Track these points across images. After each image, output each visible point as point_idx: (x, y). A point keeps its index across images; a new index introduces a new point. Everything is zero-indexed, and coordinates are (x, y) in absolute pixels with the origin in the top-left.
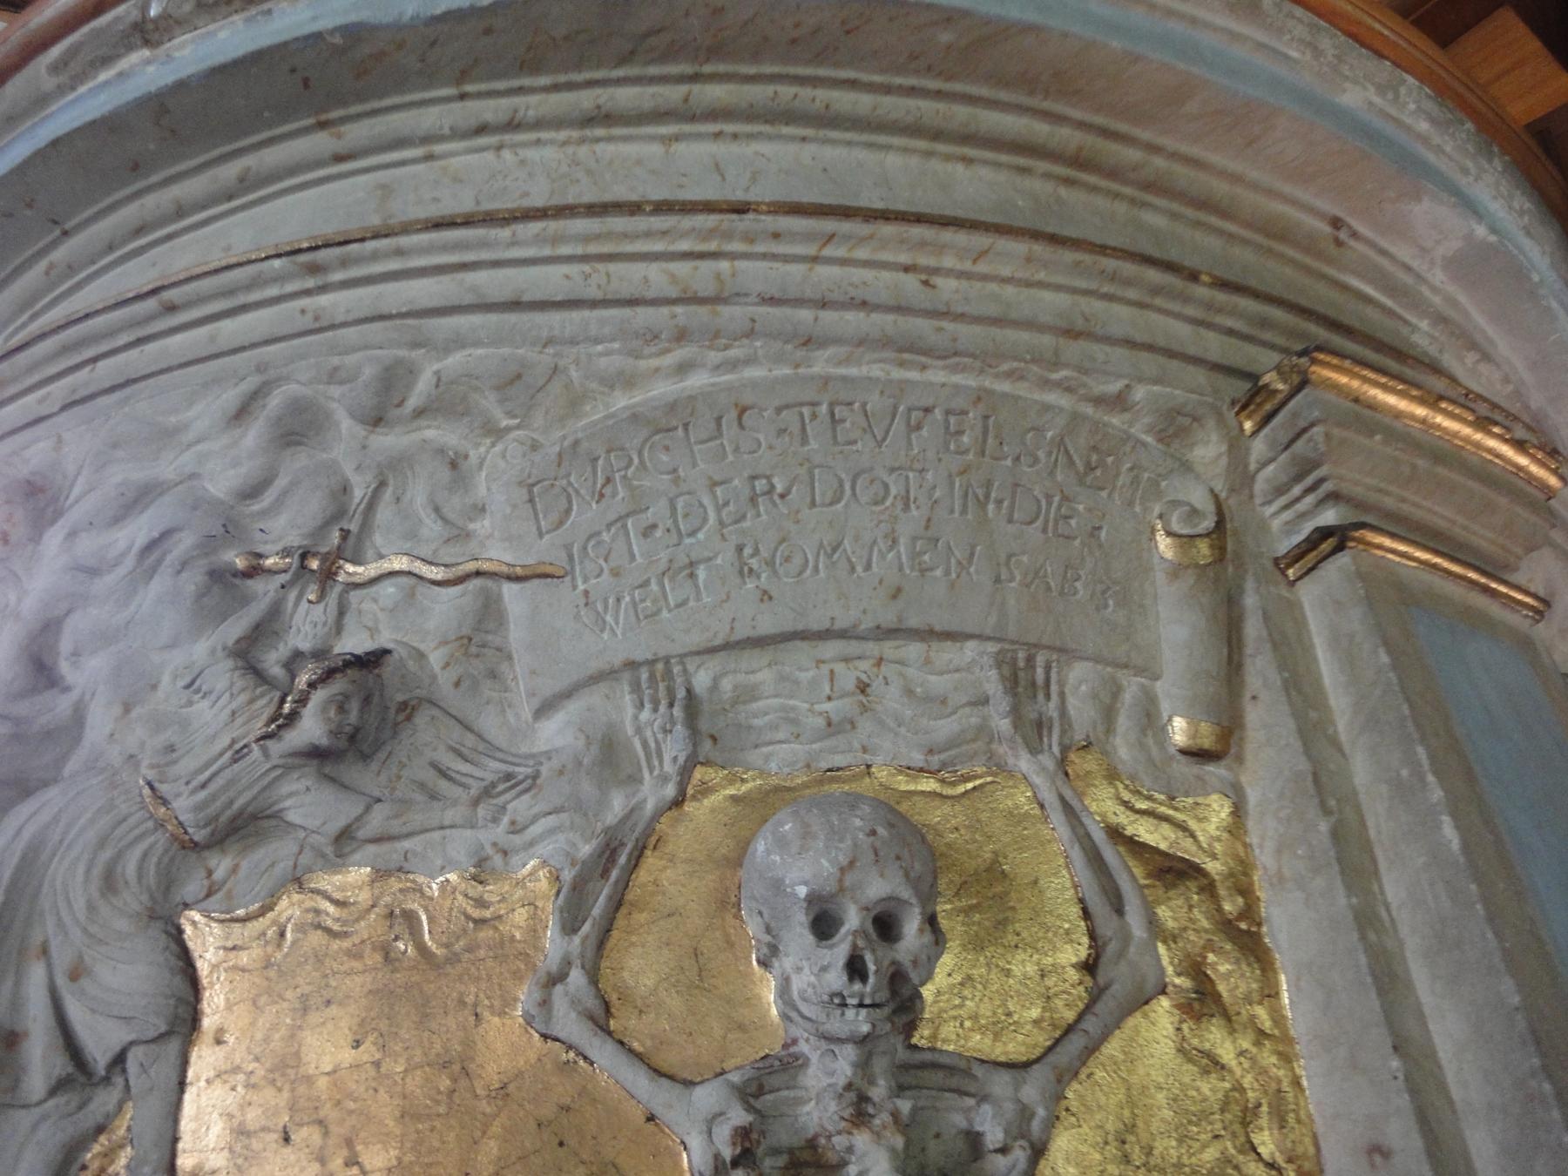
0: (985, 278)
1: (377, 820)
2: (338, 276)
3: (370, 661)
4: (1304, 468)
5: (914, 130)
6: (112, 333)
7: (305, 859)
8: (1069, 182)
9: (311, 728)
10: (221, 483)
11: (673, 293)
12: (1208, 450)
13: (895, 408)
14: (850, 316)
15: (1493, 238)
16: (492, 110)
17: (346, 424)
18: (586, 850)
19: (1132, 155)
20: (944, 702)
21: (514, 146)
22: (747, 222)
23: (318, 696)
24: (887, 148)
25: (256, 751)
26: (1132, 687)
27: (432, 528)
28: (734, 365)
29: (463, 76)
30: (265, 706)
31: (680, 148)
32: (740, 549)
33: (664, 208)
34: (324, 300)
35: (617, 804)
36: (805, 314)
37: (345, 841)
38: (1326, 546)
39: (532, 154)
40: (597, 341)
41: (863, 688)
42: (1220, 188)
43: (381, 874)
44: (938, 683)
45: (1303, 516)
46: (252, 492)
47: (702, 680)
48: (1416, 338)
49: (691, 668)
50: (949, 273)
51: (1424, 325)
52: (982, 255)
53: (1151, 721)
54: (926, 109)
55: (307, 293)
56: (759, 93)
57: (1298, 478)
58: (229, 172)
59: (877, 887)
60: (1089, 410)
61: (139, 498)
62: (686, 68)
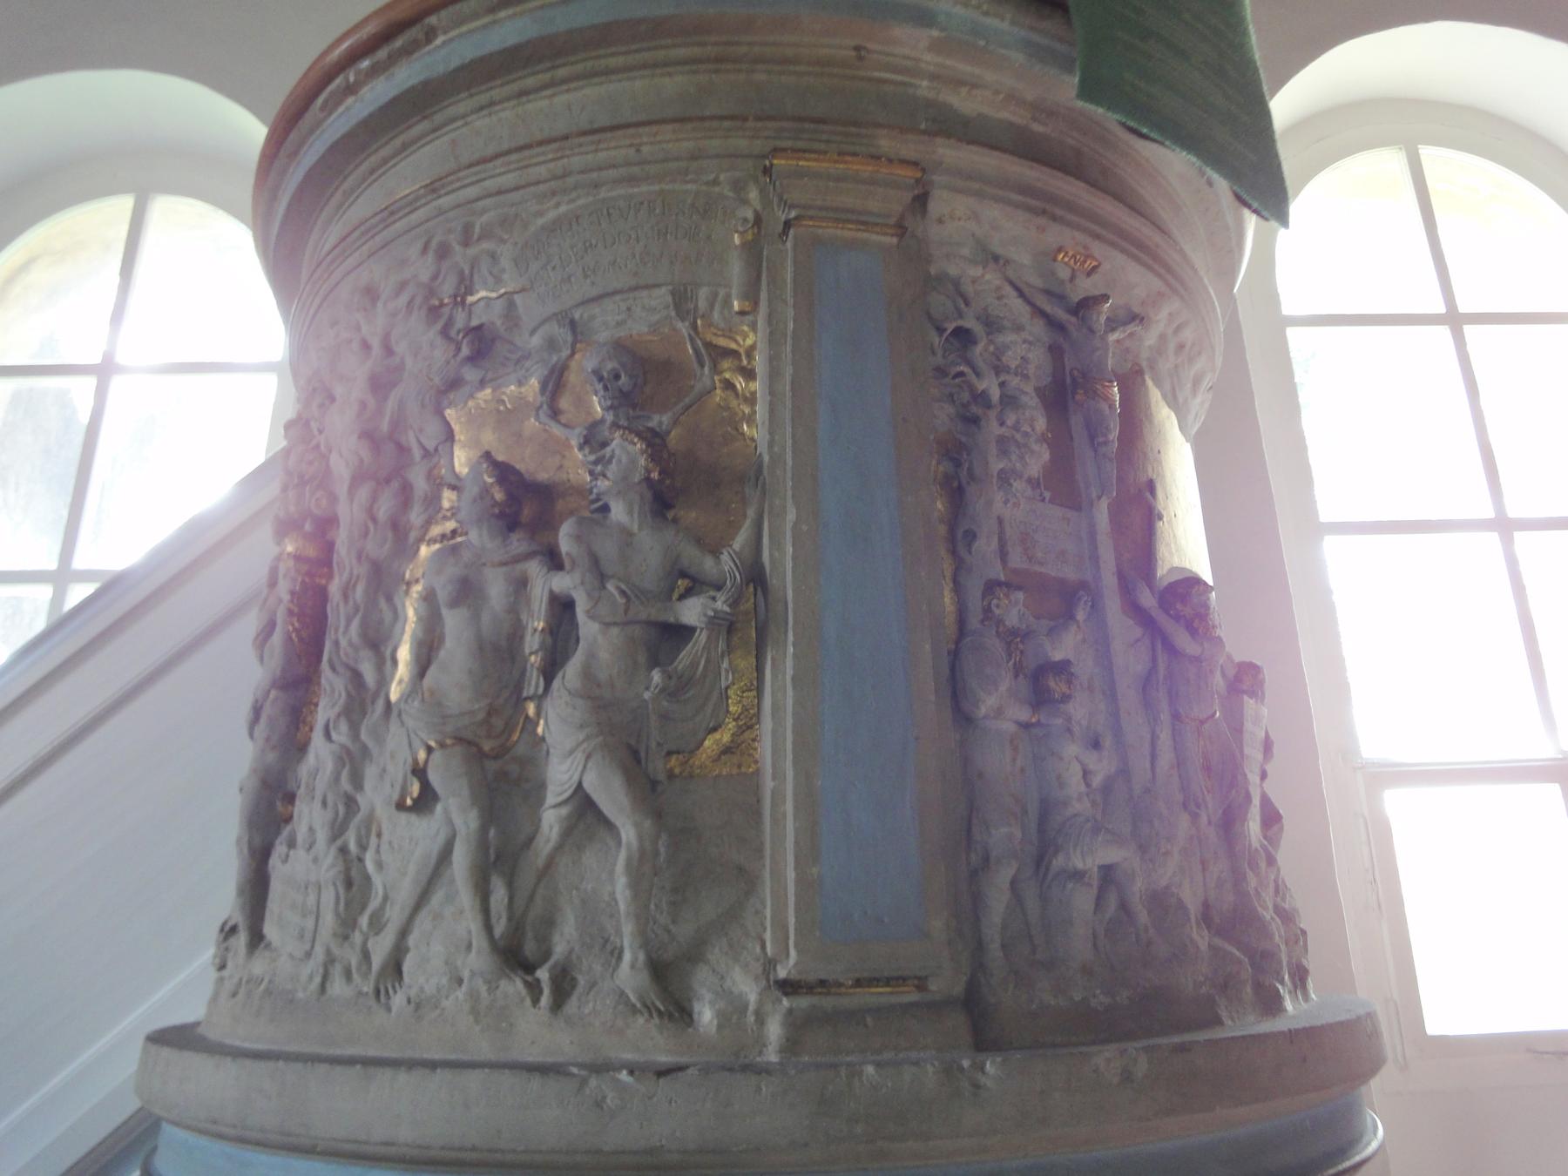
0: (660, 142)
2: (443, 192)
3: (479, 328)
5: (644, 66)
6: (377, 225)
8: (717, 71)
9: (465, 351)
10: (425, 277)
12: (753, 194)
13: (630, 205)
14: (610, 172)
15: (943, 34)
16: (483, 99)
17: (458, 248)
18: (546, 373)
19: (743, 49)
20: (655, 309)
23: (465, 341)
25: (452, 361)
26: (722, 292)
27: (491, 280)
28: (573, 201)
30: (453, 347)
31: (556, 100)
32: (584, 269)
33: (541, 143)
34: (441, 201)
35: (555, 358)
36: (595, 175)
37: (482, 384)
39: (503, 115)
41: (629, 309)
43: (494, 390)
44: (653, 303)
46: (435, 277)
47: (577, 316)
48: (919, 92)
49: (573, 311)
50: (646, 143)
51: (925, 83)
53: (727, 303)
54: (646, 56)
56: (579, 68)
58: (398, 142)
59: (610, 365)
60: (704, 188)
61: (402, 286)
62: (548, 65)
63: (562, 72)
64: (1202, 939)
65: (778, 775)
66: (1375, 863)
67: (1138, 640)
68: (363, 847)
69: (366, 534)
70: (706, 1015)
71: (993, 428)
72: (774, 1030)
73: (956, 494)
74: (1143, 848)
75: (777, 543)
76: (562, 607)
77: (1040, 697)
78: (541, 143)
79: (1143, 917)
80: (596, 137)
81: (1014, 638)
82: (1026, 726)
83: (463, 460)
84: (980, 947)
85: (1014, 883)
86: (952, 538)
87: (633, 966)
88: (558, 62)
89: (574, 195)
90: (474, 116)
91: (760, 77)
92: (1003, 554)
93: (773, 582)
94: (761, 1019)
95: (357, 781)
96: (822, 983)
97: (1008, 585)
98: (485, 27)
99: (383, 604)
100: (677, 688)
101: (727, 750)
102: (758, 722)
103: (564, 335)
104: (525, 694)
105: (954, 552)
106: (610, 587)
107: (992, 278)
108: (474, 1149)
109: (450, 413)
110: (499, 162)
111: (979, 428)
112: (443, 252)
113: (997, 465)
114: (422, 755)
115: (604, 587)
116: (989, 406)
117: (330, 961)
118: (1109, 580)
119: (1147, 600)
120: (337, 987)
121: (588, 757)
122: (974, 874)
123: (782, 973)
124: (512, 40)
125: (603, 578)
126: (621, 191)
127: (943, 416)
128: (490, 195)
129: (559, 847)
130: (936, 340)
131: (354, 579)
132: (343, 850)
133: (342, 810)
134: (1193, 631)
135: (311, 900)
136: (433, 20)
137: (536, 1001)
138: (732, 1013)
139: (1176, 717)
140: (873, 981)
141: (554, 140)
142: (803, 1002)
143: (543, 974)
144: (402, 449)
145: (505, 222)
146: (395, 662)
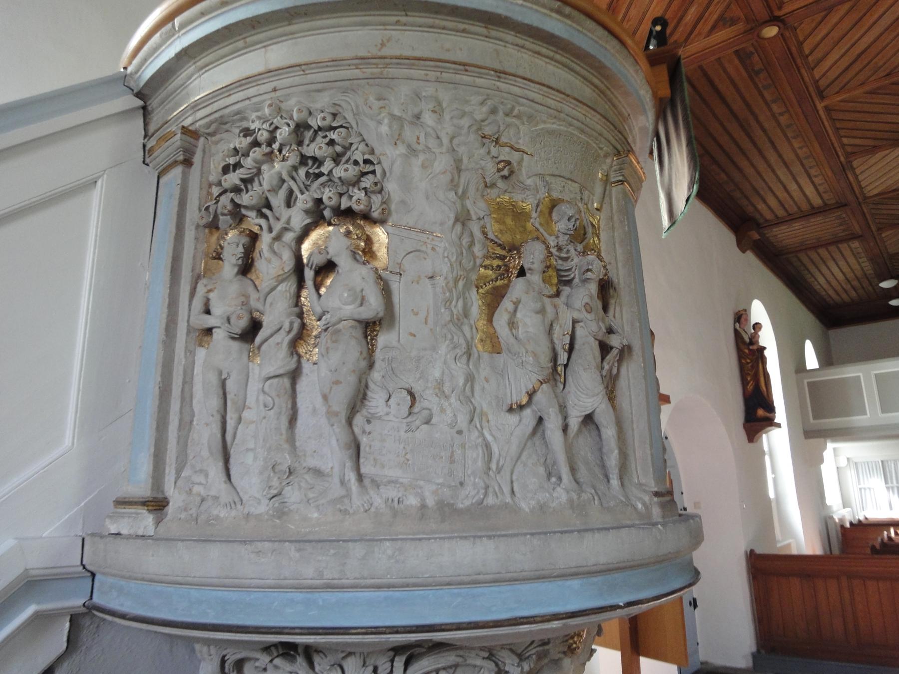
1: (510, 190)
4: (621, 169)
7: (500, 193)
11: (555, 108)
17: (501, 113)
21: (521, 52)
22: (568, 99)
24: (577, 79)
28: (559, 125)
29: (519, 32)
31: (548, 65)
33: (558, 91)
38: (620, 183)
39: (524, 55)
40: (543, 113)
42: (617, 103)
45: (617, 176)
52: (594, 116)
55: (495, 80)
56: (564, 60)
57: (619, 170)
58: (461, 26)
63: (558, 57)
78: (558, 91)
80: (578, 103)
88: (559, 51)
89: (561, 123)
90: (510, 46)
98: (545, 14)
110: (538, 86)
112: (494, 111)
124: (557, 32)
128: (527, 99)
131: (459, 277)
141: (564, 94)
145: (531, 117)
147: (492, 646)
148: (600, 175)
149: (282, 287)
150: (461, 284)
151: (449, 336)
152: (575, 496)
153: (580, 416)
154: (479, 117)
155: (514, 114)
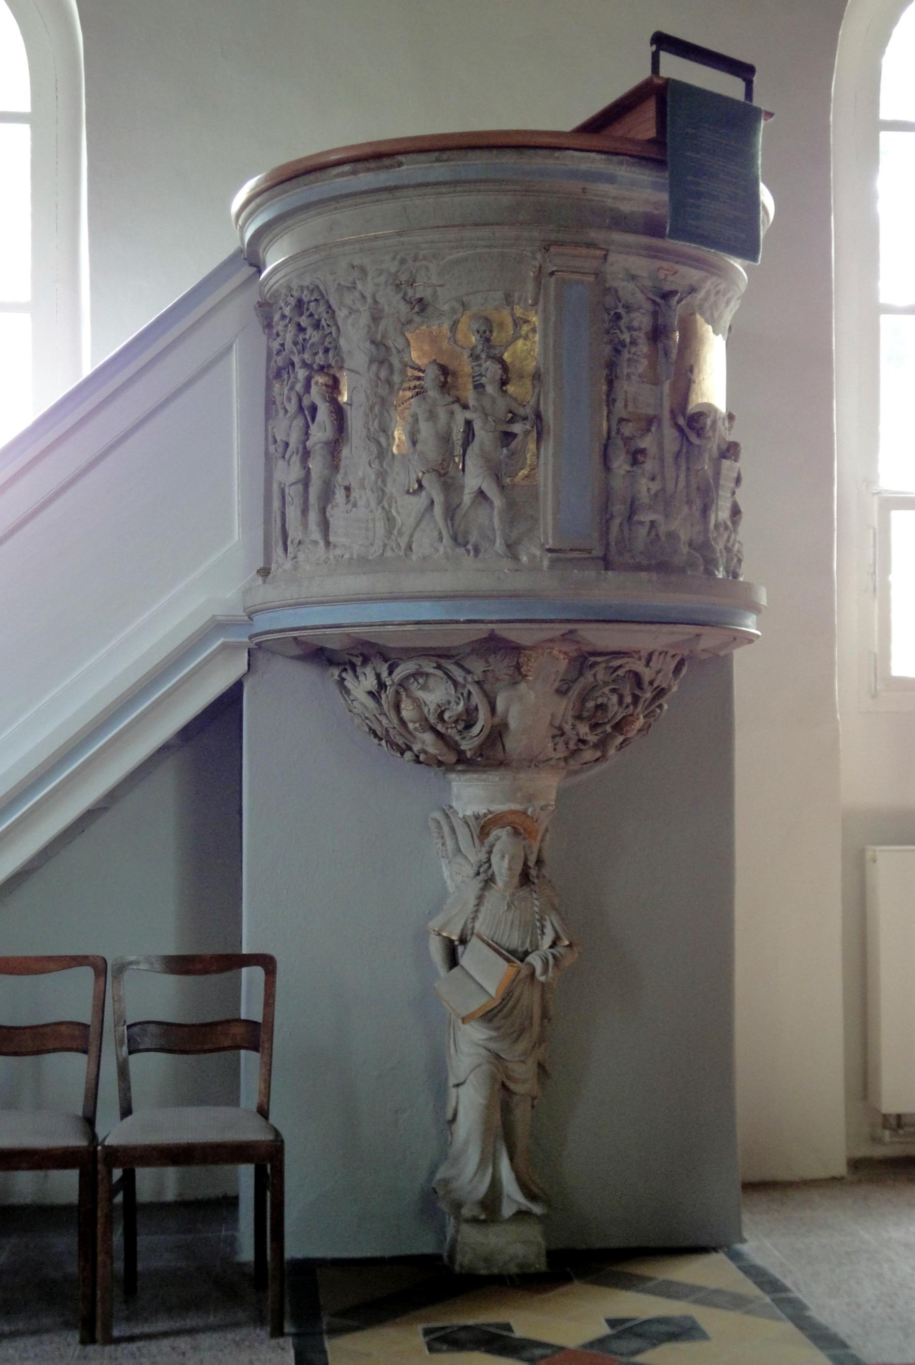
9: (416, 309)
12: (539, 256)
17: (410, 262)
28: (465, 251)
47: (464, 300)
53: (526, 300)
59: (483, 328)
64: (685, 549)
65: (545, 486)
66: (877, 560)
67: (676, 438)
68: (390, 507)
69: (377, 386)
70: (524, 559)
71: (626, 355)
72: (546, 563)
73: (610, 382)
74: (667, 516)
75: (546, 403)
76: (469, 424)
77: (635, 462)
79: (663, 538)
81: (627, 440)
82: (629, 472)
83: (416, 356)
84: (608, 544)
85: (621, 524)
86: (608, 401)
87: (500, 544)
91: (542, 199)
92: (626, 406)
93: (544, 417)
94: (541, 561)
95: (384, 482)
96: (560, 550)
97: (628, 421)
99: (386, 414)
100: (512, 454)
101: (527, 477)
102: (537, 467)
103: (457, 306)
104: (455, 454)
105: (608, 405)
106: (490, 418)
107: (631, 286)
108: (462, 591)
109: (408, 335)
111: (620, 355)
112: (403, 261)
113: (625, 371)
114: (420, 474)
115: (487, 419)
116: (624, 346)
117: (385, 546)
118: (666, 415)
119: (681, 421)
120: (389, 554)
121: (484, 478)
122: (607, 521)
123: (547, 547)
125: (486, 415)
126: (487, 250)
127: (607, 350)
129: (469, 508)
130: (606, 317)
132: (383, 508)
133: (380, 493)
134: (699, 435)
135: (371, 526)
136: (402, 158)
137: (469, 555)
138: (532, 557)
139: (688, 469)
140: (576, 550)
142: (554, 555)
143: (470, 547)
144: (388, 348)
146: (394, 438)
147: (387, 647)
148: (531, 274)
149: (295, 423)
150: (377, 408)
151: (367, 447)
152: (449, 551)
153: (472, 493)
154: (393, 270)
155: (420, 258)
